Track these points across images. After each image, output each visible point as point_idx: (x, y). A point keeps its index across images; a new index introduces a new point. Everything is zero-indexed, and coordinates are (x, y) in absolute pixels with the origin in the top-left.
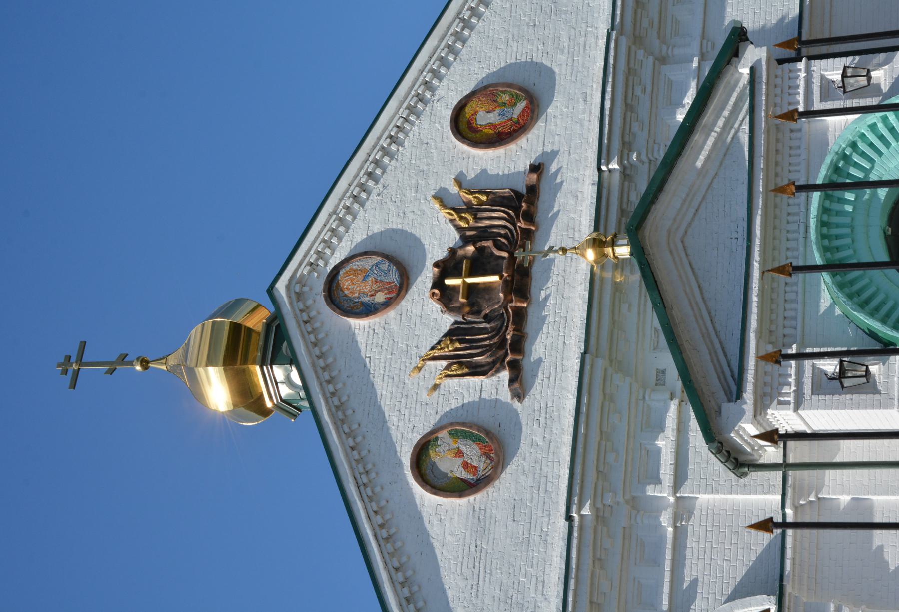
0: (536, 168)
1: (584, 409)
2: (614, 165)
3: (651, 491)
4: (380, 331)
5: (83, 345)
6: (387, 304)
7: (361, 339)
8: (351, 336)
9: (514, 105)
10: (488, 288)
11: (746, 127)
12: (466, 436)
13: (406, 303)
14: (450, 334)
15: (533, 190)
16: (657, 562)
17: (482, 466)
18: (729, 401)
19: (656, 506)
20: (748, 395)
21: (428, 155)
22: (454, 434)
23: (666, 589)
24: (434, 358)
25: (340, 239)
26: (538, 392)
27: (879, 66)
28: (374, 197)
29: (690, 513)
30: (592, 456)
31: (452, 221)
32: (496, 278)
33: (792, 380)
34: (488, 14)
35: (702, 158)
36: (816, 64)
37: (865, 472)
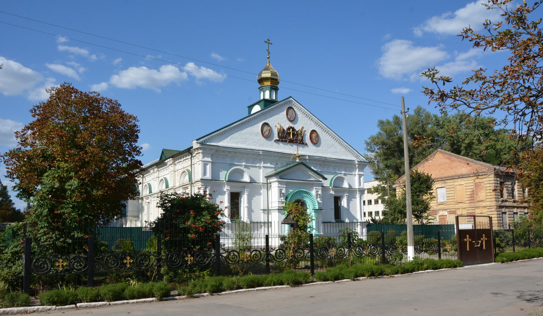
0: (306, 144)
3: (262, 163)
5: (271, 44)
6: (288, 118)
7: (283, 113)
8: (283, 111)
11: (313, 180)
13: (288, 122)
14: (284, 130)
15: (303, 144)
19: (260, 164)
20: (280, 180)
21: (309, 125)
23: (249, 165)
26: (275, 144)
28: (303, 115)
29: (259, 168)
30: (268, 154)
32: (292, 137)
36: (321, 190)
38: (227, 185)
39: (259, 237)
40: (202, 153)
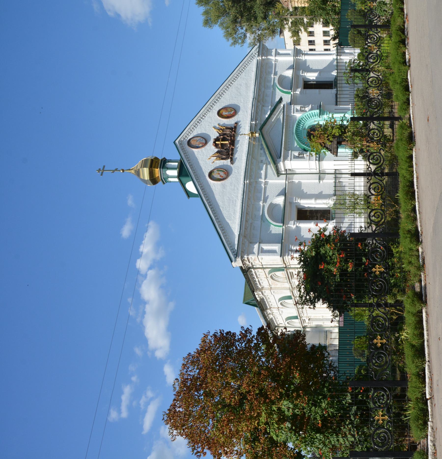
0: (236, 123)
1: (247, 164)
2: (254, 123)
3: (260, 180)
4: (200, 152)
6: (202, 146)
7: (196, 153)
8: (193, 152)
9: (231, 111)
10: (225, 144)
12: (220, 171)
13: (207, 147)
14: (217, 152)
15: (235, 127)
16: (261, 192)
17: (224, 176)
18: (278, 158)
19: (261, 182)
20: (282, 158)
22: (218, 170)
23: (263, 197)
24: (213, 157)
25: (191, 134)
26: (236, 163)
27: (307, 107)
28: (199, 126)
30: (249, 172)
31: (217, 132)
32: (227, 142)
33: (290, 156)
34: (225, 94)
35: (273, 119)
37: (301, 175)
38: (288, 224)
39: (353, 185)
40: (248, 255)
